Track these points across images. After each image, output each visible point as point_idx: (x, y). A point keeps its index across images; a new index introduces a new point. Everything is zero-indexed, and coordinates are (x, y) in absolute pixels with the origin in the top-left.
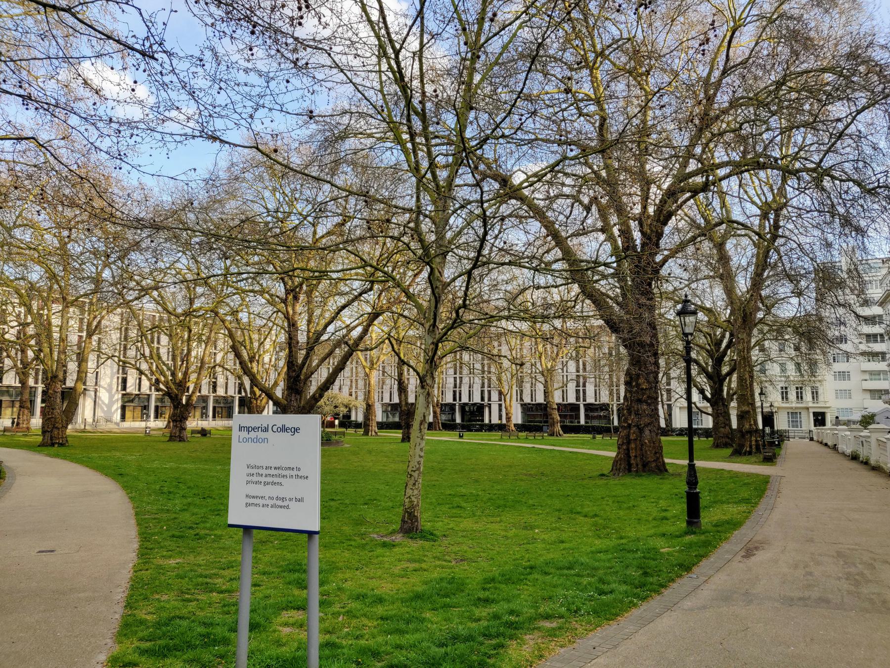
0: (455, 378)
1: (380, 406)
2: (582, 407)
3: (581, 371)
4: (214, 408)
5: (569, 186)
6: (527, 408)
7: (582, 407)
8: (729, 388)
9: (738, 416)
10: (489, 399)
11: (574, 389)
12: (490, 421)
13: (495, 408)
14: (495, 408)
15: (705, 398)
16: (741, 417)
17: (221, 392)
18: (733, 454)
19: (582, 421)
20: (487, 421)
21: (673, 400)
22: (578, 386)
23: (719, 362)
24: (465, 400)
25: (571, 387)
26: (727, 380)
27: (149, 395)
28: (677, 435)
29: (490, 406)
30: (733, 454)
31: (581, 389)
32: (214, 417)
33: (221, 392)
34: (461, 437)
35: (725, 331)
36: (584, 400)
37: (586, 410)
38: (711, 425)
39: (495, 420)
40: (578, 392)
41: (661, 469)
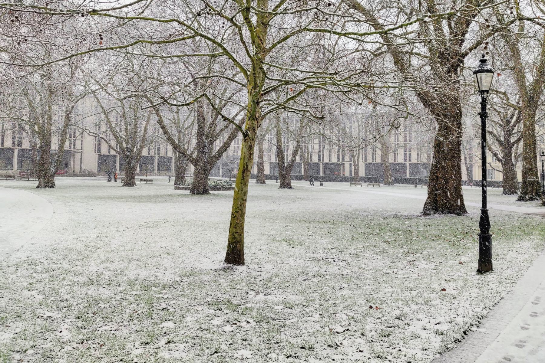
0: (320, 145)
1: (364, 165)
2: (408, 165)
3: (396, 141)
4: (159, 164)
5: (457, 16)
6: (368, 166)
7: (408, 165)
8: (516, 153)
9: (523, 172)
10: (343, 160)
11: (403, 153)
12: (344, 175)
13: (347, 166)
14: (347, 166)
15: (498, 159)
16: (525, 174)
17: (163, 154)
18: (519, 200)
19: (408, 176)
20: (341, 175)
21: (474, 162)
22: (405, 151)
23: (509, 134)
24: (326, 160)
25: (401, 152)
26: (515, 147)
27: (171, 158)
28: (474, 185)
29: (343, 164)
30: (519, 200)
31: (408, 153)
32: (159, 170)
33: (163, 154)
34: (322, 185)
35: (515, 109)
36: (410, 160)
37: (411, 168)
38: (501, 179)
39: (347, 174)
40: (405, 155)
41: (461, 210)
